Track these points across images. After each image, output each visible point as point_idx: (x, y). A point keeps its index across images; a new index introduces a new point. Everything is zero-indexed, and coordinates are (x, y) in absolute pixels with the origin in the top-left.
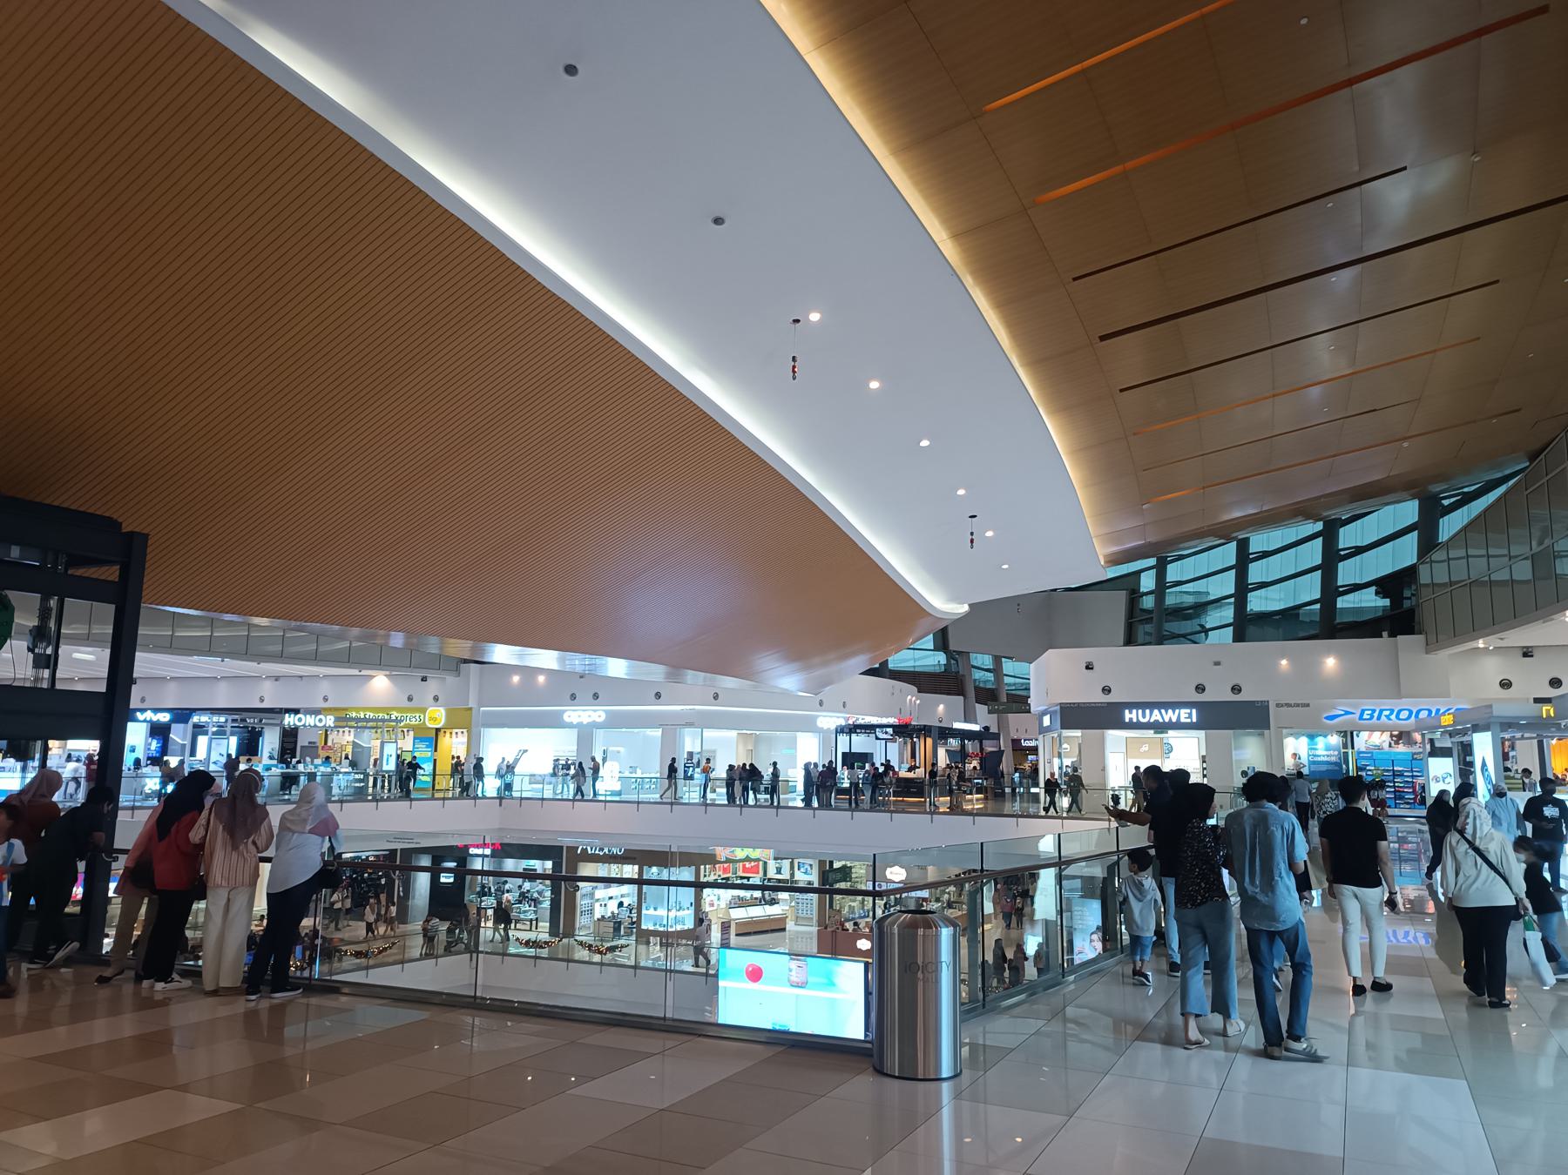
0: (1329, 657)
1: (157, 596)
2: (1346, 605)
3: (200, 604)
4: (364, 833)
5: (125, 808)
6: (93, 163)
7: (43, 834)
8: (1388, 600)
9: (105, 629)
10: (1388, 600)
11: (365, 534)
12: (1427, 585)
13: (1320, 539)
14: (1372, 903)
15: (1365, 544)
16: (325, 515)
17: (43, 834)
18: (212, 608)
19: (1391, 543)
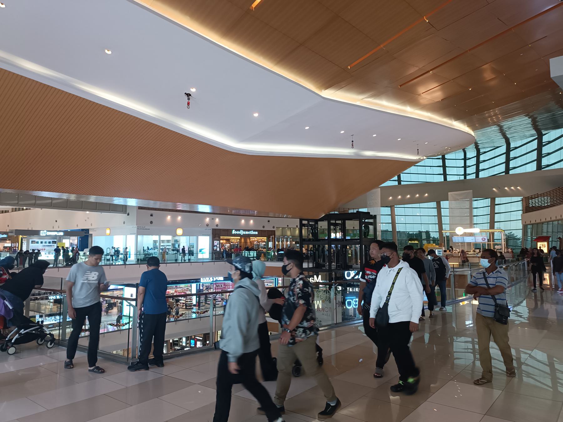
0: (206, 219)
1: (77, 191)
2: (25, 248)
3: (76, 192)
4: (311, 154)
5: (102, 334)
6: (22, 124)
7: (143, 317)
8: (303, 223)
9: (465, 234)
10: (303, 223)
11: (126, 176)
12: (471, 204)
13: (505, 155)
14: (487, 264)
15: (551, 152)
16: (128, 175)
17: (143, 317)
18: (84, 193)
19: (560, 151)
